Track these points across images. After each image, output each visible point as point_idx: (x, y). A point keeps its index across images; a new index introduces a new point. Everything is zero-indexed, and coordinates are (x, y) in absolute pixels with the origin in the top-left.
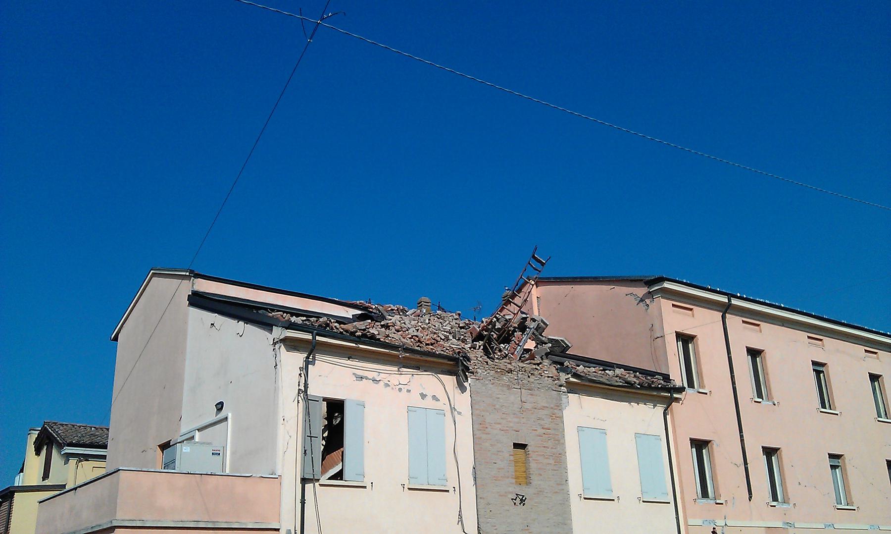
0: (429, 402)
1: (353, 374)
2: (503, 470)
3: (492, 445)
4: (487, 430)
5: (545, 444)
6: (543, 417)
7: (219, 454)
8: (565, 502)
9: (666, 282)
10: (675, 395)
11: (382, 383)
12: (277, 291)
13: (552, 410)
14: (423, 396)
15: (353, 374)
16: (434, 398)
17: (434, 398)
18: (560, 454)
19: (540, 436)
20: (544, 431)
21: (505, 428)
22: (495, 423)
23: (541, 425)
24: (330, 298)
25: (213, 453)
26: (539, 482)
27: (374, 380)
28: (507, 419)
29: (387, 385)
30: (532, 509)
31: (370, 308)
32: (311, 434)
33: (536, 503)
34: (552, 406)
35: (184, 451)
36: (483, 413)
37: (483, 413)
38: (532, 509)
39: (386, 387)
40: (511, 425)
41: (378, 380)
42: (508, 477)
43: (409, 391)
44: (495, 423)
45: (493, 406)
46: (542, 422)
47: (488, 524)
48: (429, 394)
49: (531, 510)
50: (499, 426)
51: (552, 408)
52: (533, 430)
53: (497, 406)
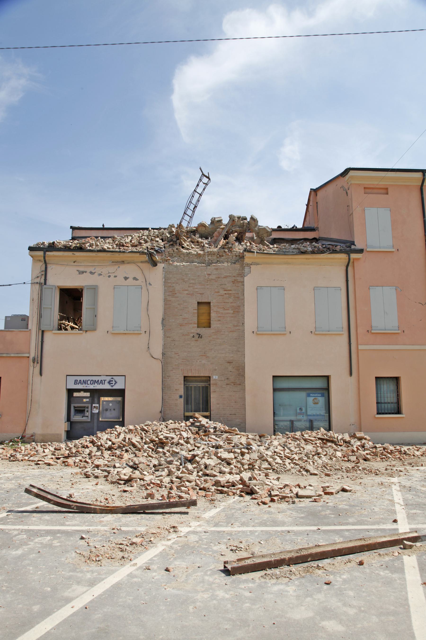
0: (130, 281)
1: (77, 271)
4: (176, 295)
5: (227, 301)
7: (25, 320)
8: (241, 337)
11: (96, 274)
13: (234, 278)
14: (126, 278)
15: (77, 271)
16: (135, 279)
17: (135, 279)
20: (225, 292)
21: (191, 293)
23: (224, 288)
25: (22, 320)
27: (91, 273)
29: (100, 275)
31: (36, 547)
32: (213, 384)
33: (213, 338)
35: (7, 319)
40: (197, 290)
41: (93, 272)
43: (115, 277)
44: (182, 290)
48: (131, 276)
50: (187, 292)
51: (234, 276)
52: (215, 292)
53: (186, 280)
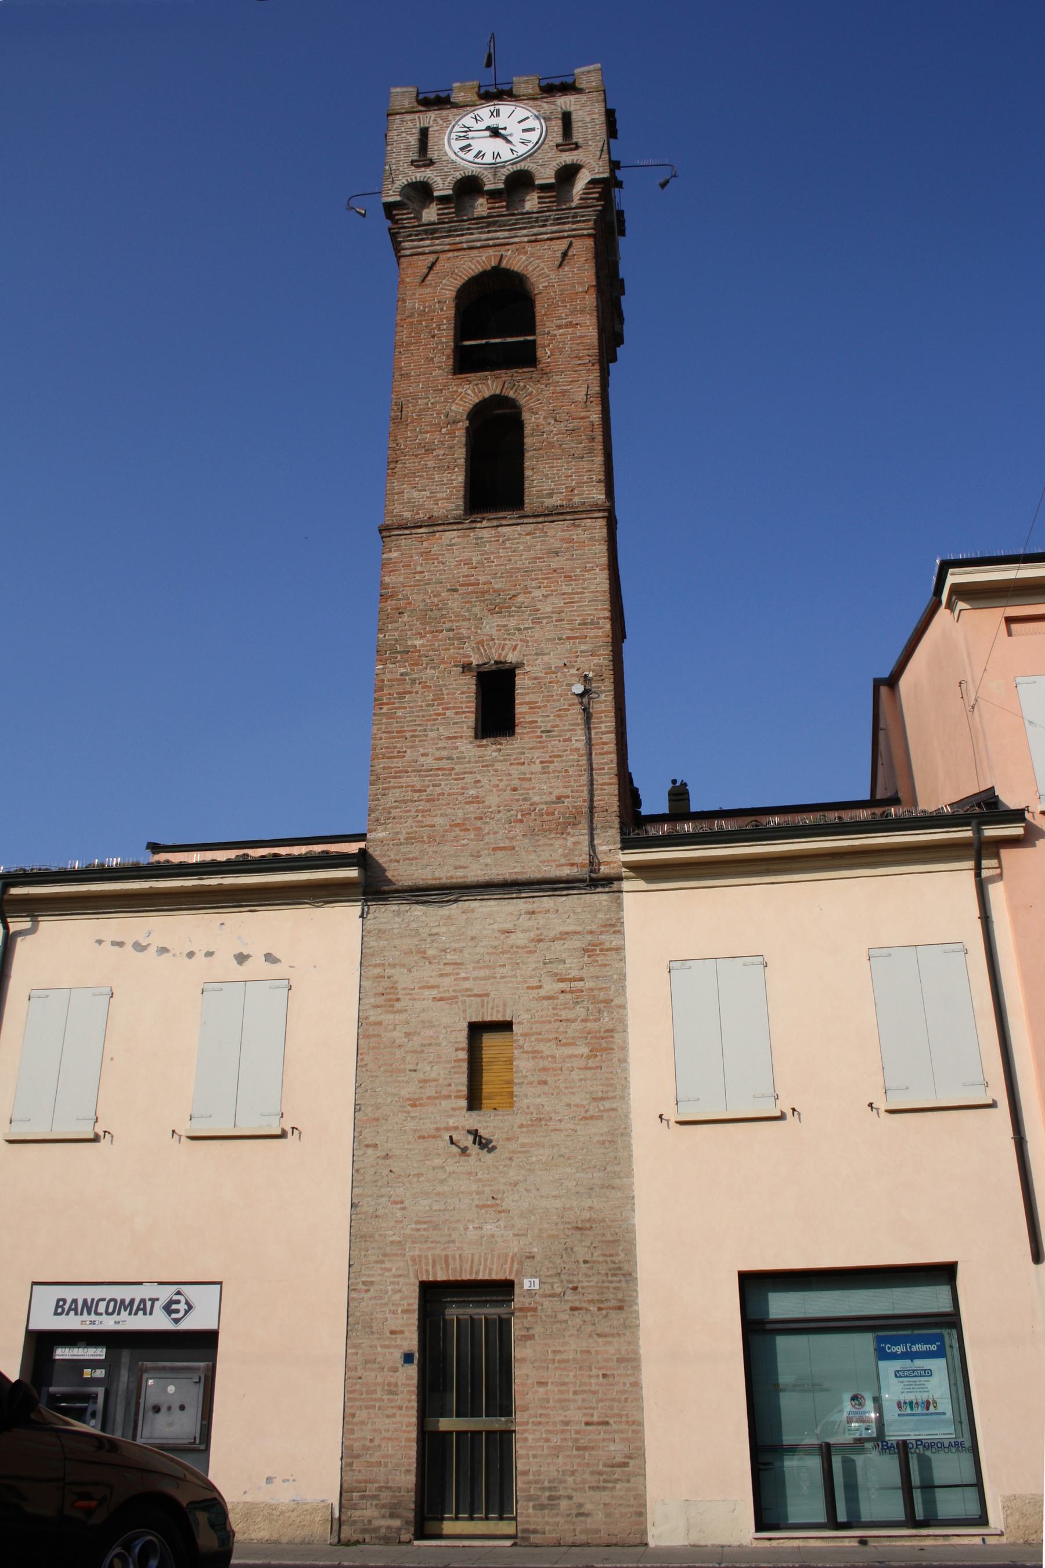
2: (434, 1084)
3: (408, 1035)
6: (564, 956)
9: (951, 571)
10: (970, 834)
11: (152, 950)
12: (326, 840)
14: (241, 958)
18: (607, 1031)
19: (549, 998)
20: (563, 986)
22: (420, 988)
23: (556, 974)
24: (934, 579)
26: (539, 1100)
28: (458, 974)
29: (163, 950)
30: (511, 1159)
33: (523, 1145)
34: (594, 927)
36: (389, 971)
37: (389, 971)
38: (511, 1159)
39: (161, 954)
40: (467, 985)
42: (449, 1097)
44: (420, 988)
45: (420, 953)
46: (559, 968)
47: (384, 1200)
49: (508, 1162)
52: (528, 988)
